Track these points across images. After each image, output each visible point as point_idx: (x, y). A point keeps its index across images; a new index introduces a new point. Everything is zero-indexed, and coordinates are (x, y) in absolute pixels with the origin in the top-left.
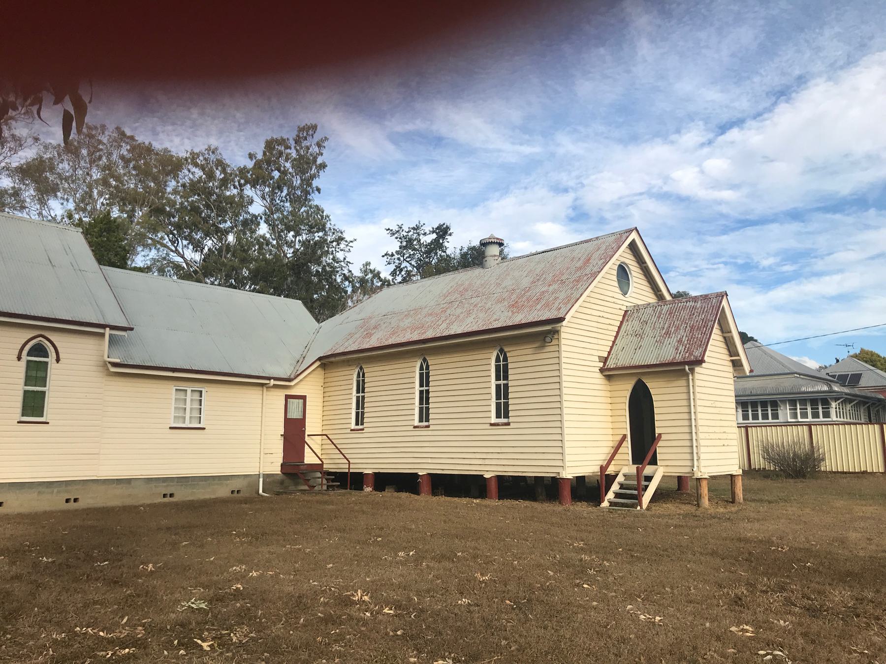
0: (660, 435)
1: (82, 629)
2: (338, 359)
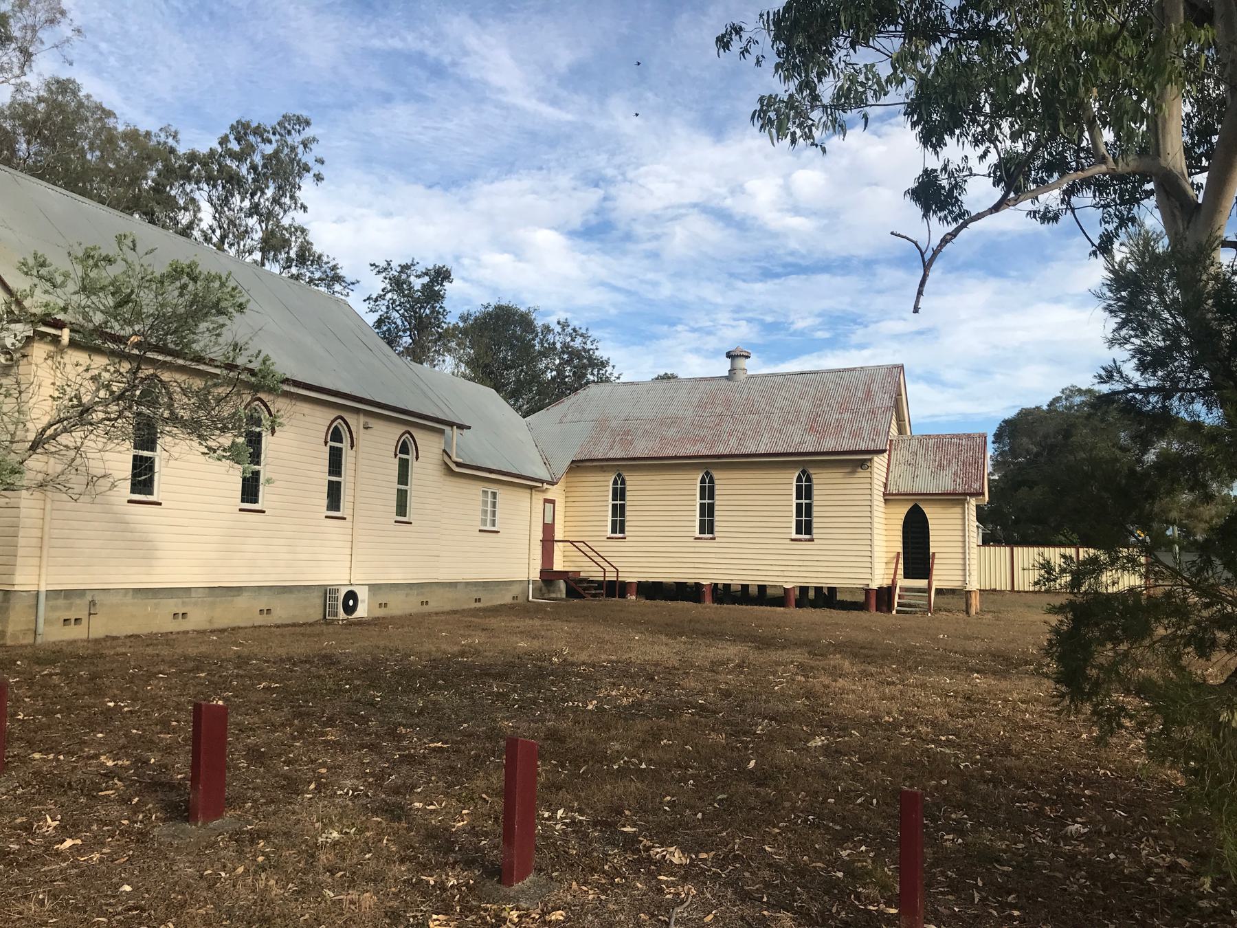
0: (934, 553)
2: (595, 464)
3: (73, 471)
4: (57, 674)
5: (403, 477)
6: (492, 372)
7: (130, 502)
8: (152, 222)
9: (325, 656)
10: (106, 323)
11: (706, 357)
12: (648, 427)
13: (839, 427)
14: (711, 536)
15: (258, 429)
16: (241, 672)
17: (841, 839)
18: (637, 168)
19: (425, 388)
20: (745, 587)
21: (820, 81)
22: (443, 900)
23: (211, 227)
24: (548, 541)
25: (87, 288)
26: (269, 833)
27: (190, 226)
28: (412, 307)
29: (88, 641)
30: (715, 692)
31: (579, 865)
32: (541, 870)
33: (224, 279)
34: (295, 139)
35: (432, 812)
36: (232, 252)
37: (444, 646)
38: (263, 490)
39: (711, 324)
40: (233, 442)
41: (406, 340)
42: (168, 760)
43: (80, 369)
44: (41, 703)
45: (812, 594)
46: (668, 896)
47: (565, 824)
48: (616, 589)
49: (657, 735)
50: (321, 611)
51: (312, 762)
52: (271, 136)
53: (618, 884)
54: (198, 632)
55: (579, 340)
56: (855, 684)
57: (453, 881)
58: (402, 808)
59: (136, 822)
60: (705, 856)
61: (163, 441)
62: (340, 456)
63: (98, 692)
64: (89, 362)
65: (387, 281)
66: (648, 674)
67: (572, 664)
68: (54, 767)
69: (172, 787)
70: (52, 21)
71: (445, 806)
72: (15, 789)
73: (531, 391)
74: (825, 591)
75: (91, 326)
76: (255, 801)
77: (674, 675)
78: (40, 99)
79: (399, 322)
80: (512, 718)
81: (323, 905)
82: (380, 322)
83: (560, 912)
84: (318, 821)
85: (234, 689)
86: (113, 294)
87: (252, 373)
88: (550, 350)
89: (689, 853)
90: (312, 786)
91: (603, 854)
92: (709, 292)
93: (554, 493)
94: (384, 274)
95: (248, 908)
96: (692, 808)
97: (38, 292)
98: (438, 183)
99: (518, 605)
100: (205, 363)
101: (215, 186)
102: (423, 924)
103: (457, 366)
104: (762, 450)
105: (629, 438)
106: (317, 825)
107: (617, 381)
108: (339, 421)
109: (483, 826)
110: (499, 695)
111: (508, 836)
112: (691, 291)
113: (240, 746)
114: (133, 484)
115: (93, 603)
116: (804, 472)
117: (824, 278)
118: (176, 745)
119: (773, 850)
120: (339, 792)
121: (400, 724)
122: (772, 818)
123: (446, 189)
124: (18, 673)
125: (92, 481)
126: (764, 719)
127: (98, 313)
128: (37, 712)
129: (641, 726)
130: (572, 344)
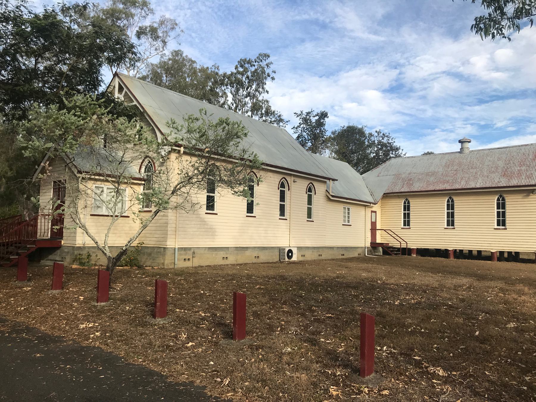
1: (20, 309)
2: (395, 194)
3: (187, 202)
4: (183, 280)
5: (310, 202)
6: (346, 156)
7: (206, 213)
8: (210, 103)
9: (281, 276)
10: (196, 144)
11: (450, 143)
12: (420, 177)
13: (520, 173)
14: (453, 227)
15: (253, 184)
16: (249, 281)
17: (525, 372)
18: (415, 58)
19: (318, 164)
20: (470, 252)
21: (505, 5)
22: (335, 380)
23: (232, 103)
24: (374, 230)
25: (189, 131)
26: (263, 346)
27: (224, 104)
28: (311, 130)
29: (193, 267)
30: (457, 299)
31: (394, 371)
32: (377, 372)
33: (239, 124)
34: (264, 64)
35: (329, 343)
36: (240, 112)
37: (329, 274)
38: (255, 208)
39: (452, 127)
40: (244, 189)
41: (309, 144)
42: (224, 315)
43: (188, 162)
44: (177, 290)
45: (506, 255)
46: (437, 390)
47: (387, 353)
48: (407, 251)
49: (429, 317)
50: (278, 257)
51: (279, 319)
52: (254, 63)
53: (413, 381)
54: (232, 265)
55: (386, 139)
56: (531, 299)
57: (339, 373)
58: (316, 341)
59: (214, 338)
60: (455, 373)
61: (218, 190)
62: (284, 194)
63: (197, 287)
64: (191, 159)
65: (301, 120)
66: (424, 290)
67: (387, 284)
68: (184, 315)
69: (226, 325)
70: (173, 28)
71: (334, 342)
72: (171, 322)
73: (364, 163)
74: (513, 254)
75: (191, 145)
76: (257, 333)
77: (436, 291)
78: (170, 59)
79: (306, 137)
80: (362, 306)
81: (286, 377)
82: (298, 137)
83: (387, 391)
84: (282, 343)
85: (247, 288)
86: (199, 132)
87: (251, 161)
88: (372, 144)
89: (447, 371)
90: (279, 329)
91: (405, 367)
92: (451, 112)
93: (375, 208)
94: (300, 117)
95: (257, 375)
96: (447, 351)
97: (173, 133)
98: (324, 75)
99: (361, 257)
100: (233, 158)
101: (233, 87)
102: (327, 389)
103: (331, 154)
104: (478, 186)
105: (411, 182)
106: (282, 345)
107: (405, 156)
108: (284, 179)
109: (351, 351)
110: (354, 296)
111: (363, 355)
112: (442, 112)
113: (250, 311)
114: (207, 207)
115: (194, 253)
116: (501, 196)
117: (512, 101)
118: (226, 309)
119: (490, 374)
120: (290, 332)
121: (313, 306)
122: (489, 359)
123: (328, 77)
124: (169, 279)
125: (193, 205)
126: (483, 312)
127: (194, 140)
128: (176, 294)
129: (421, 313)
130: (382, 141)
